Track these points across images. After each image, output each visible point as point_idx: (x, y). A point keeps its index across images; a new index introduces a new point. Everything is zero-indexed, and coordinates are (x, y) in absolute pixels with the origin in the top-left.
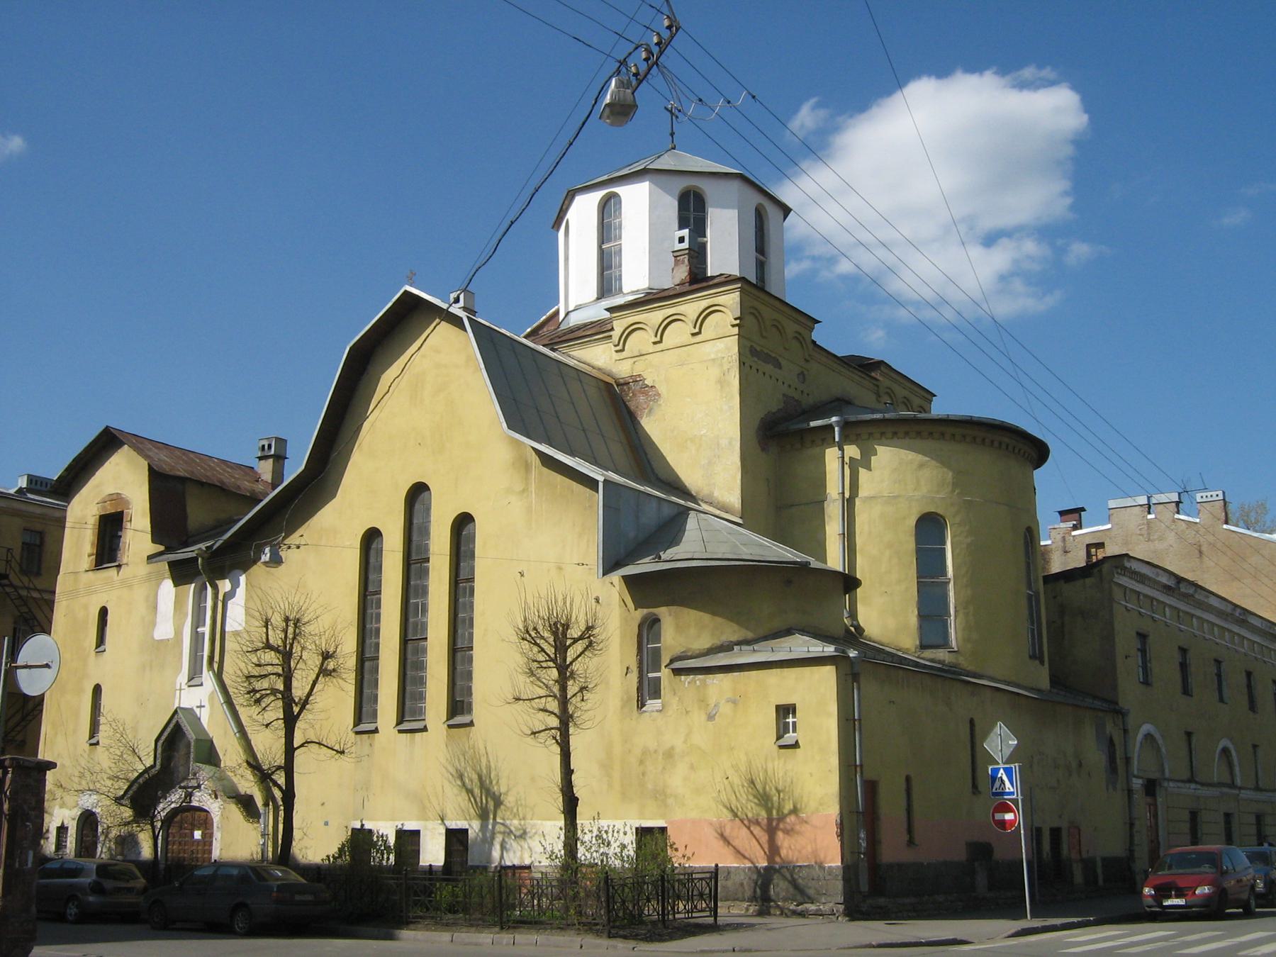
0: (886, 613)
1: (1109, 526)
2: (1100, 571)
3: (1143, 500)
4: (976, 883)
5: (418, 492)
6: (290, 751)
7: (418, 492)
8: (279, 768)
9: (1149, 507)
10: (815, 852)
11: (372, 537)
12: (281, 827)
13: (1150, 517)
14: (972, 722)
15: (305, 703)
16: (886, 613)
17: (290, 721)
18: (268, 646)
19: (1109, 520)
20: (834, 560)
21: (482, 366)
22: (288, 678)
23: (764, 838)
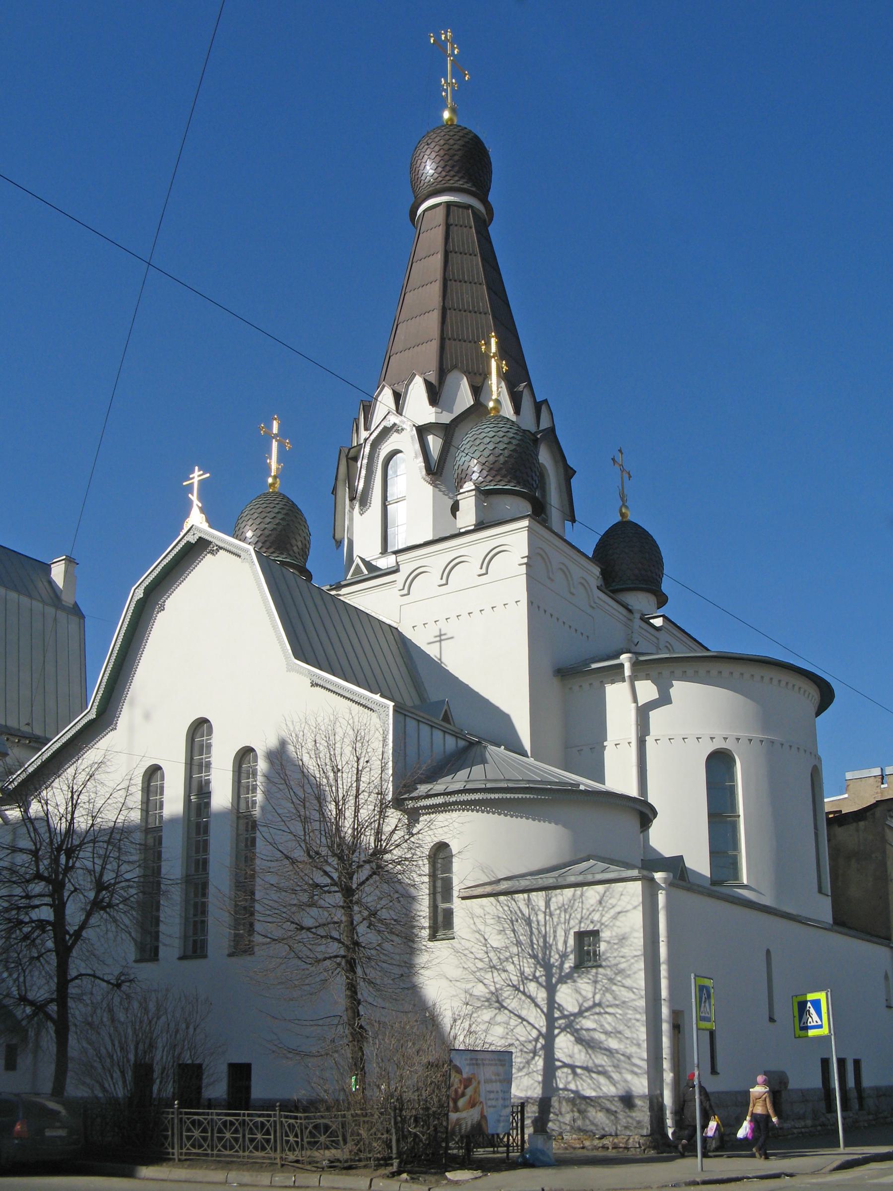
0: (680, 831)
1: (846, 796)
2: (873, 814)
3: (877, 772)
4: (797, 1125)
5: (200, 728)
6: (63, 982)
7: (200, 728)
8: (52, 1000)
9: (883, 778)
10: (421, 950)
11: (154, 772)
12: (666, 1041)
13: (883, 786)
14: (768, 952)
15: (78, 935)
16: (680, 831)
17: (63, 952)
18: (38, 876)
19: (846, 790)
20: (620, 777)
21: (290, 651)
22: (59, 908)
23: (541, 995)
